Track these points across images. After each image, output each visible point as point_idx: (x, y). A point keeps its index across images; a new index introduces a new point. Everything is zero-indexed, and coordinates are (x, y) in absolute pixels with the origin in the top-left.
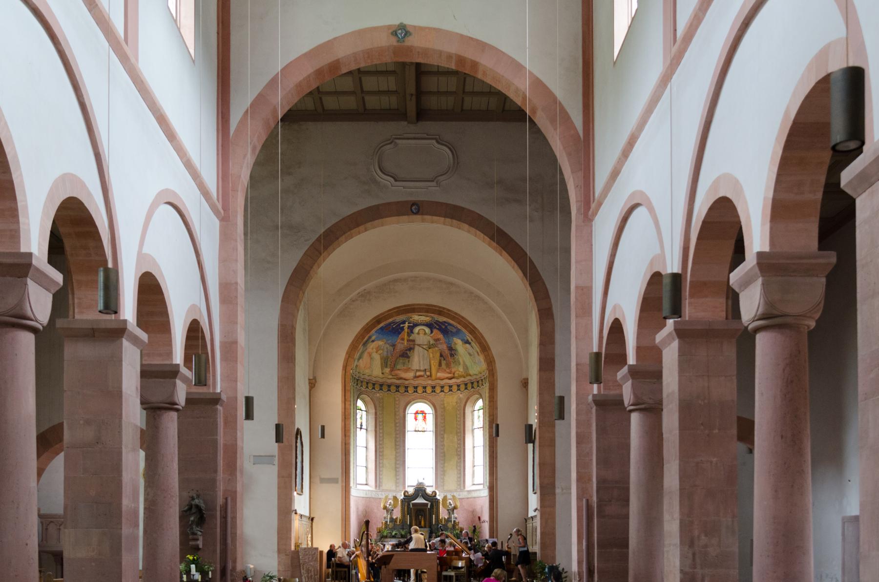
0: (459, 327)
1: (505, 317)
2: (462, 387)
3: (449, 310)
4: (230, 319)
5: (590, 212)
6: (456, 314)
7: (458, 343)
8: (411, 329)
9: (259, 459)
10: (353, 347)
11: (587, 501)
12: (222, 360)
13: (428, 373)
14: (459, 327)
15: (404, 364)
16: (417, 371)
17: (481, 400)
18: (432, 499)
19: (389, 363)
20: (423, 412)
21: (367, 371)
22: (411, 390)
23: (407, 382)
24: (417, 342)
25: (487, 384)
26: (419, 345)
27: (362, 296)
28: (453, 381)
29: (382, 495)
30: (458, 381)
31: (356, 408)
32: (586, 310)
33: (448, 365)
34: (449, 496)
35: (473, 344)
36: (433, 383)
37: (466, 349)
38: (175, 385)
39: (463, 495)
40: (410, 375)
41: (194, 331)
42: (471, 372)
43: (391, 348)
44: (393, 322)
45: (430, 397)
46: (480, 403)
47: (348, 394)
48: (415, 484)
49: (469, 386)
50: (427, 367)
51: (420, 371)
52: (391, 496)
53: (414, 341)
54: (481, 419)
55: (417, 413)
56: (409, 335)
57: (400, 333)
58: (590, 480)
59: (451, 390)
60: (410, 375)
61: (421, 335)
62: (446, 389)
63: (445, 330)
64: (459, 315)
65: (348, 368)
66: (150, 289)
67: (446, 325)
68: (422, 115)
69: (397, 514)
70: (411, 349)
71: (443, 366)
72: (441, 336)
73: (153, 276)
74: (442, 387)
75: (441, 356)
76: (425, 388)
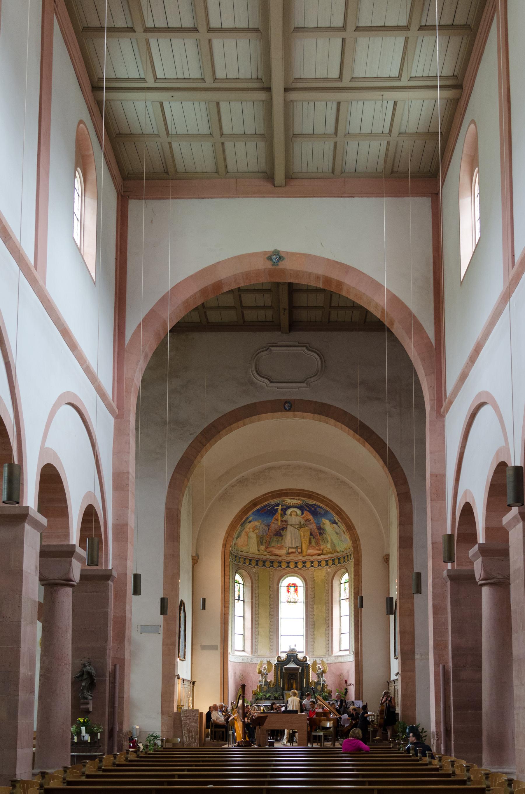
2: (330, 562)
4: (121, 504)
5: (442, 410)
7: (326, 523)
8: (284, 510)
9: (145, 629)
10: (232, 527)
11: (444, 666)
12: (114, 540)
15: (278, 541)
16: (290, 548)
18: (303, 663)
19: (264, 541)
20: (294, 585)
21: (245, 549)
22: (284, 565)
23: (280, 558)
24: (289, 523)
25: (353, 560)
26: (291, 525)
27: (240, 482)
29: (257, 661)
30: (327, 557)
31: (234, 581)
32: (440, 495)
33: (317, 543)
34: (318, 661)
35: (339, 524)
36: (304, 559)
38: (71, 562)
39: (331, 660)
40: (283, 552)
41: (90, 515)
42: (338, 549)
43: (267, 528)
45: (301, 572)
46: (346, 577)
47: (227, 569)
48: (287, 650)
49: (337, 561)
50: (298, 545)
51: (292, 548)
52: (265, 661)
53: (286, 521)
54: (347, 591)
55: (289, 586)
57: (274, 515)
58: (446, 647)
59: (319, 565)
60: (283, 552)
62: (316, 564)
66: (51, 480)
67: (315, 508)
68: (294, 326)
69: (271, 678)
70: (284, 529)
71: (313, 543)
72: (311, 517)
73: (54, 467)
74: (312, 562)
75: (311, 534)
76: (296, 563)
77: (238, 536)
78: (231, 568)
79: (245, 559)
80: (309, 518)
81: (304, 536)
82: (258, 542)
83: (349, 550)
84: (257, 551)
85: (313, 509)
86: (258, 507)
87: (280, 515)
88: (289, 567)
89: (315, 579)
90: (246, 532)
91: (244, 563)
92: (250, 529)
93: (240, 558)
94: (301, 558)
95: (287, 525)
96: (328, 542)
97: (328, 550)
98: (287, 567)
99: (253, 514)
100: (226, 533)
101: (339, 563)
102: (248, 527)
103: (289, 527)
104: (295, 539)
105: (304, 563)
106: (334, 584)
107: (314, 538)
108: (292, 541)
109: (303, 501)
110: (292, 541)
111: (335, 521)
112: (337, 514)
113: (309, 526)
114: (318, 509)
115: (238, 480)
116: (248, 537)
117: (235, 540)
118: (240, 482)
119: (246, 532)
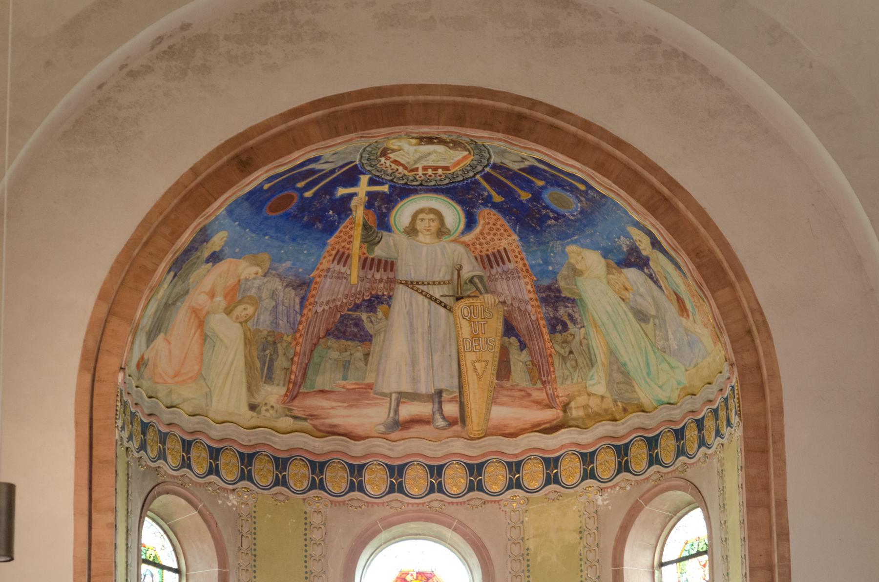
0: (601, 184)
1: (806, 133)
2: (606, 462)
3: (556, 112)
6: (587, 126)
7: (587, 268)
8: (381, 207)
10: (114, 304)
13: (451, 409)
14: (601, 184)
15: (346, 365)
16: (403, 397)
17: (697, 515)
19: (281, 362)
21: (188, 394)
22: (376, 481)
23: (357, 449)
24: (404, 272)
25: (735, 434)
26: (411, 285)
27: (171, 52)
28: (564, 437)
30: (586, 438)
33: (540, 372)
35: (659, 262)
36: (474, 451)
37: (623, 293)
40: (371, 416)
42: (645, 395)
43: (291, 297)
44: (303, 172)
45: (461, 513)
46: (692, 528)
47: (103, 479)
49: (639, 454)
50: (446, 381)
51: (414, 397)
53: (389, 265)
56: (370, 239)
57: (330, 229)
59: (552, 479)
61: (424, 238)
62: (533, 474)
63: (522, 203)
64: (602, 133)
65: (109, 363)
67: (534, 190)
70: (376, 302)
71: (519, 374)
72: (508, 240)
75: (509, 329)
76: (436, 471)
77: (158, 328)
78: (122, 478)
79: (187, 446)
80: (504, 244)
81: (475, 336)
82: (249, 365)
83: (719, 381)
84: (244, 408)
85: (525, 196)
86: (257, 178)
87: (358, 232)
88: (401, 490)
89: (531, 544)
90: (195, 311)
91: (186, 463)
92: (212, 295)
93: (163, 438)
94: (459, 446)
95: (392, 281)
96: (592, 364)
97: (594, 403)
98: (391, 490)
99: (230, 212)
100: (101, 297)
101: (654, 460)
102: (207, 284)
103: (402, 294)
104: (431, 352)
105: (475, 470)
106: (627, 567)
107: (523, 346)
108: (414, 363)
109: (478, 148)
110: (414, 363)
111: (634, 249)
112: (652, 209)
113: (502, 286)
114: (551, 196)
115: (160, 39)
116: (205, 338)
117: (141, 338)
118: (171, 52)
119: (195, 311)
